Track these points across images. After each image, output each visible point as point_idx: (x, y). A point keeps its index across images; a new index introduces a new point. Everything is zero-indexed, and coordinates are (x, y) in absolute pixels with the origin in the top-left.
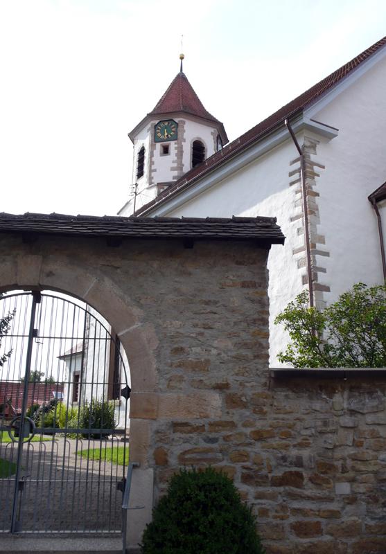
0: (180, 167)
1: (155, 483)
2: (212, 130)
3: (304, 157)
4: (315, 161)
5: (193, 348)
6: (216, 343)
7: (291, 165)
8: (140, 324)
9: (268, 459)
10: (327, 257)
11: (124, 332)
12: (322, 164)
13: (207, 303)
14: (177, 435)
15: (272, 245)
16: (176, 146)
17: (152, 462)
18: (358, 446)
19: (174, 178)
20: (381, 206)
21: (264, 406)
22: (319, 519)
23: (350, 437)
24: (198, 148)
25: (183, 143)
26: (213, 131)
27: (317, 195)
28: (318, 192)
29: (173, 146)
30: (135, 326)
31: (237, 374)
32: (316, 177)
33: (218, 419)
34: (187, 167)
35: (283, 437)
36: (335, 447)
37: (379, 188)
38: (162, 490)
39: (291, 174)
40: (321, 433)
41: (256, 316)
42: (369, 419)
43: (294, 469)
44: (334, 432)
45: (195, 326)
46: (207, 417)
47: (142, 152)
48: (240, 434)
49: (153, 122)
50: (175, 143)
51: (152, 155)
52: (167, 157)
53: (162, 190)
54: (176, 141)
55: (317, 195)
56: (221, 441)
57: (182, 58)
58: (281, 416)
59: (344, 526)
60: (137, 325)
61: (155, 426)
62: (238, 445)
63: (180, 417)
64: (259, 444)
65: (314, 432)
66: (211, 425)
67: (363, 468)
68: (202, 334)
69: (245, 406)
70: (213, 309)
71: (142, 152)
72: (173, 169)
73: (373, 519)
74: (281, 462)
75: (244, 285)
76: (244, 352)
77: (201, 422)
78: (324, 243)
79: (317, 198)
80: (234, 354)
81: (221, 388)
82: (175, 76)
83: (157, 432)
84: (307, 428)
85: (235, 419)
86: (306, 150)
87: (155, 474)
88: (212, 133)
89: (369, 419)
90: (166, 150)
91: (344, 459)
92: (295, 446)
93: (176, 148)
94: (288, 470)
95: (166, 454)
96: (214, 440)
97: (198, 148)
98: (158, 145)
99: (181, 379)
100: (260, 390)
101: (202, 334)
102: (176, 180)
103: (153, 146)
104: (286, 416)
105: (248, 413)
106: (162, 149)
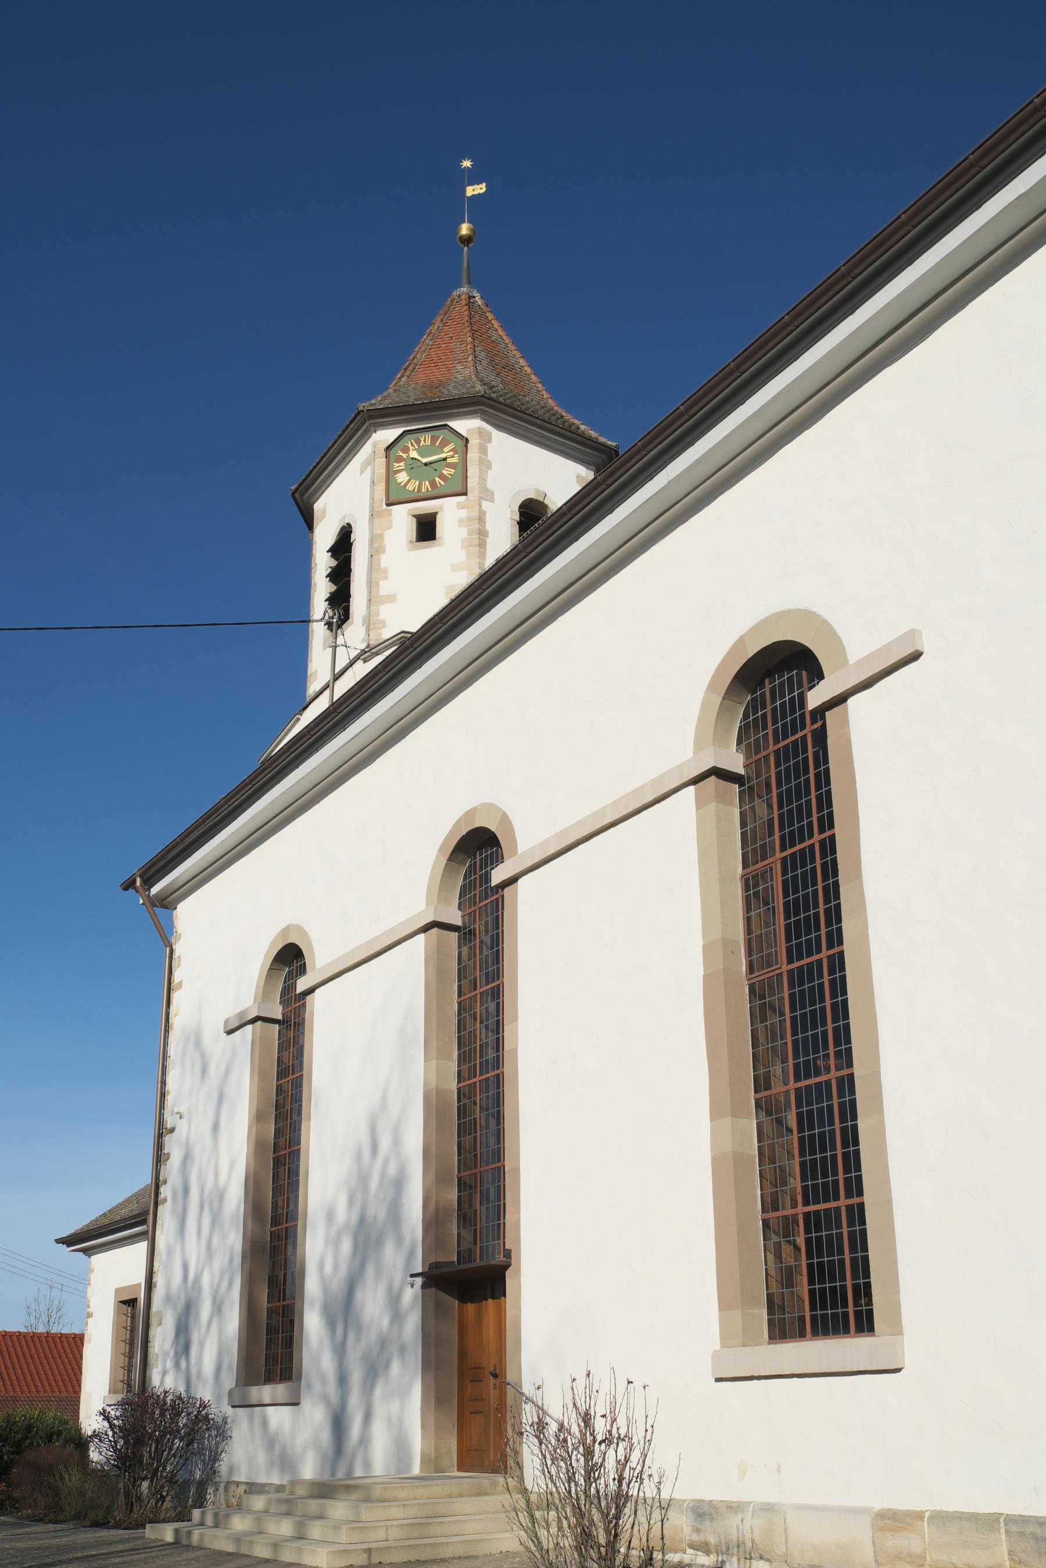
16: (464, 513)
50: (460, 506)
52: (428, 551)
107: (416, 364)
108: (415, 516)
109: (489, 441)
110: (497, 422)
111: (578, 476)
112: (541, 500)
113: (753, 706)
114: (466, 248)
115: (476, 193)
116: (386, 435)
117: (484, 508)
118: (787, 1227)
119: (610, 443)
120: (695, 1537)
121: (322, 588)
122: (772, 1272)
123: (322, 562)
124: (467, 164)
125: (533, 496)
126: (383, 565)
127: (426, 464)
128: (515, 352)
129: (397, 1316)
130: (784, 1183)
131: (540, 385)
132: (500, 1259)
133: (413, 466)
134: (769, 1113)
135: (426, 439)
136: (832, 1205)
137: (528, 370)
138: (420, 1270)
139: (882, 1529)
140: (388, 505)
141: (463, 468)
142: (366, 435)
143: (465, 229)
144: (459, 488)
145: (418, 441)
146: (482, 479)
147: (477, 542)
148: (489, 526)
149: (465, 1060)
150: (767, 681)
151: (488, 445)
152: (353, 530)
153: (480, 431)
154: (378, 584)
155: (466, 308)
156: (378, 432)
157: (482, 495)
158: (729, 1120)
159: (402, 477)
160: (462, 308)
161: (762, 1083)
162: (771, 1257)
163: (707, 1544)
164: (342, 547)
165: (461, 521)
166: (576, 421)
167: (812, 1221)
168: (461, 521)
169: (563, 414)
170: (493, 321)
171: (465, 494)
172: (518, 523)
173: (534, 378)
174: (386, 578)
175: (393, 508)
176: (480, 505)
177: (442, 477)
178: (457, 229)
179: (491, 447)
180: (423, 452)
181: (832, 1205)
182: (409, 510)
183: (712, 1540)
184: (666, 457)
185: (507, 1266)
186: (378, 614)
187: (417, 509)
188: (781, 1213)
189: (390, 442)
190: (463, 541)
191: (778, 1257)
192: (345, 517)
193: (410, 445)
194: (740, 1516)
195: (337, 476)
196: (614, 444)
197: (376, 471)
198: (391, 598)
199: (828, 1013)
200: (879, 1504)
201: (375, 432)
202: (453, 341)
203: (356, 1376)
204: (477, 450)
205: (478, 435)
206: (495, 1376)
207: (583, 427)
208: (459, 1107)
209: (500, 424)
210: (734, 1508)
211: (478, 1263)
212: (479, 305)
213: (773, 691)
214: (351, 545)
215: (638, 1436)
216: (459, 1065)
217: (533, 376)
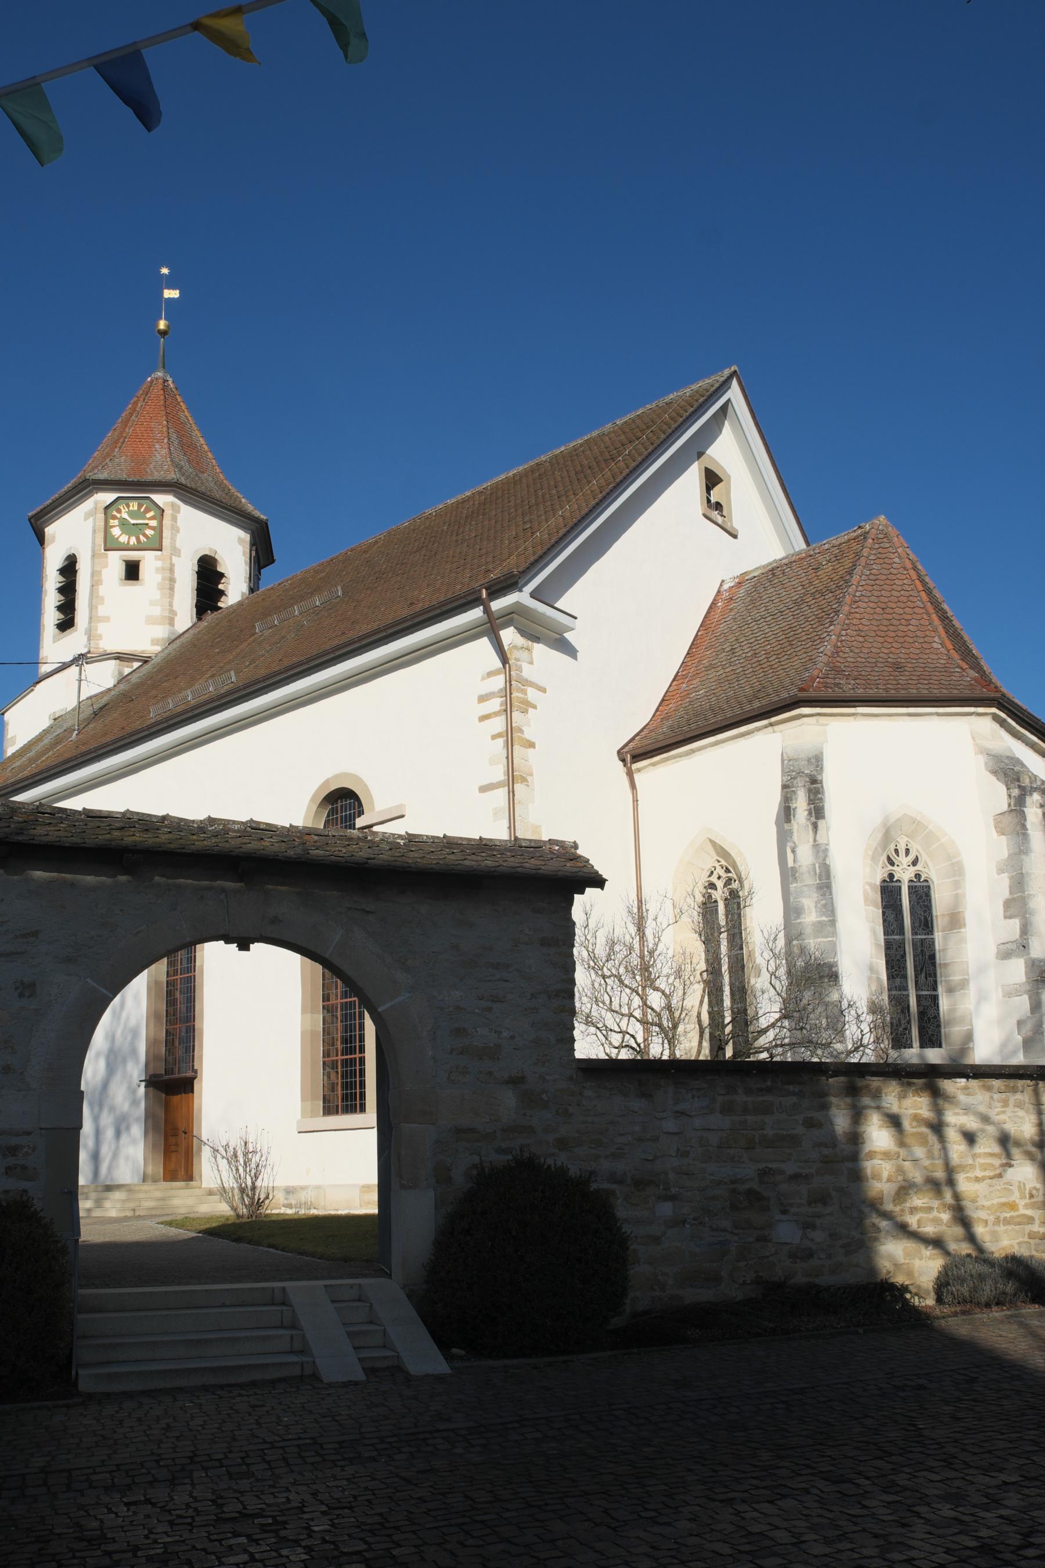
4: (529, 679)
5: (477, 1029)
7: (483, 679)
11: (388, 1005)
12: (542, 684)
15: (587, 889)
16: (159, 564)
19: (154, 642)
21: (570, 1105)
27: (531, 745)
28: (533, 740)
29: (149, 561)
30: (401, 998)
32: (530, 710)
35: (593, 1146)
37: (637, 735)
39: (482, 699)
45: (481, 998)
50: (157, 558)
51: (95, 575)
52: (132, 588)
53: (127, 671)
55: (531, 745)
65: (630, 1139)
68: (490, 1009)
72: (150, 620)
79: (531, 750)
81: (515, 1081)
84: (622, 1135)
87: (435, 1195)
89: (697, 1122)
90: (132, 571)
101: (490, 1009)
107: (125, 437)
108: (124, 561)
109: (179, 512)
110: (184, 498)
111: (239, 538)
112: (213, 556)
113: (332, 812)
114: (162, 339)
115: (171, 296)
116: (107, 497)
117: (173, 561)
118: (334, 1065)
119: (262, 517)
120: (286, 1202)
121: (51, 599)
122: (326, 1085)
123: (52, 580)
124: (165, 271)
125: (207, 553)
126: (101, 594)
127: (134, 524)
128: (197, 432)
129: (135, 1103)
130: (333, 1045)
131: (214, 461)
132: (190, 1074)
133: (123, 524)
134: (328, 1011)
135: (134, 506)
136: (353, 1056)
137: (206, 448)
138: (144, 1079)
139: (364, 1192)
140: (105, 550)
141: (159, 530)
142: (89, 494)
143: (162, 325)
144: (157, 546)
145: (128, 506)
146: (173, 540)
147: (168, 586)
148: (177, 575)
149: (171, 965)
150: (339, 801)
151: (178, 515)
152: (78, 560)
153: (173, 505)
154: (97, 608)
155: (162, 392)
156: (99, 494)
157: (172, 552)
158: (310, 1015)
159: (116, 532)
160: (157, 391)
161: (326, 998)
162: (326, 1078)
163: (291, 1204)
164: (69, 569)
165: (157, 569)
166: (239, 495)
167: (345, 1063)
168: (157, 569)
169: (230, 487)
170: (181, 403)
171: (161, 550)
172: (197, 573)
173: (210, 455)
174: (102, 604)
175: (109, 552)
176: (171, 560)
177: (145, 535)
178: (157, 325)
179: (180, 517)
180: (132, 514)
181: (353, 1056)
182: (121, 556)
183: (293, 1202)
184: (295, 678)
185: (195, 1078)
186: (96, 629)
187: (125, 556)
188: (331, 1059)
189: (108, 503)
190: (159, 584)
191: (329, 1077)
192: (71, 548)
193: (122, 508)
194: (306, 1192)
195: (65, 514)
196: (265, 518)
197: (97, 523)
198: (107, 619)
199: (164, 1290)
200: (363, 1183)
201: (97, 493)
202: (152, 420)
203: (109, 1133)
204: (170, 518)
205: (171, 508)
206: (185, 1133)
207: (243, 500)
208: (167, 991)
209: (186, 500)
210: (303, 1188)
211: (176, 1076)
212: (171, 389)
213: (342, 806)
214: (76, 571)
215: (264, 1152)
216: (168, 968)
217: (209, 453)
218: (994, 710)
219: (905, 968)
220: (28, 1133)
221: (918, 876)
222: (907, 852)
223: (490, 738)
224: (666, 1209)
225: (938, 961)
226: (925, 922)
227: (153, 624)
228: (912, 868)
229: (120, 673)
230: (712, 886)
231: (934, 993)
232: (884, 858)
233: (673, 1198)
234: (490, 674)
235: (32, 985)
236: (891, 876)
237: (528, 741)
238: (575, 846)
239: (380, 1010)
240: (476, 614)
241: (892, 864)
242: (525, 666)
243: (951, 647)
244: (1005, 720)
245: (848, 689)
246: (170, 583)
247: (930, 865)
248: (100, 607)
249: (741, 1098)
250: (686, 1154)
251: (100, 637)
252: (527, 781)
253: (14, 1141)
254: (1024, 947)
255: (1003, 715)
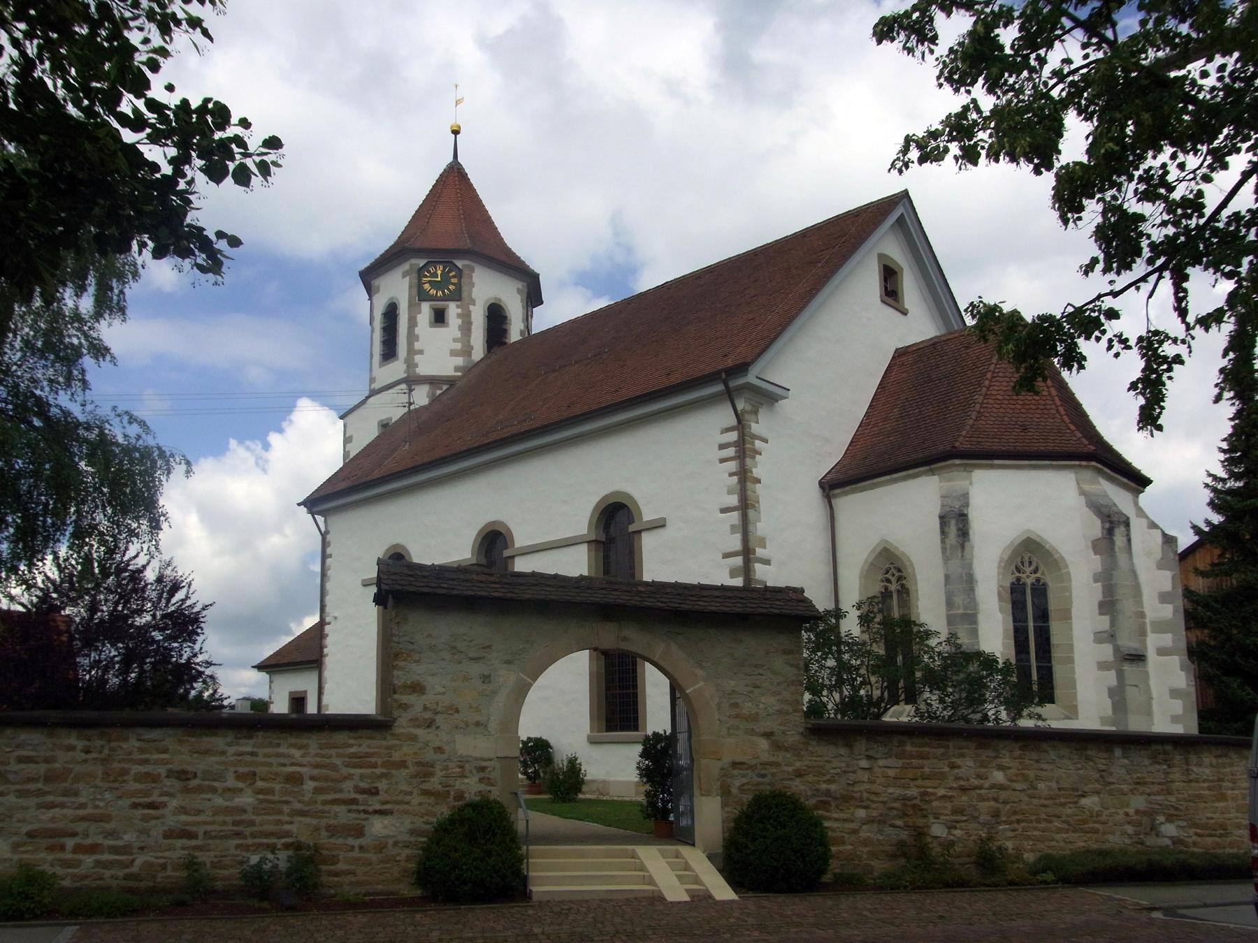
0: (467, 351)
1: (722, 807)
2: (520, 285)
3: (743, 428)
6: (763, 700)
7: (722, 433)
8: (703, 683)
9: (805, 790)
10: (768, 566)
11: (691, 689)
13: (756, 666)
14: (736, 772)
16: (459, 311)
17: (719, 791)
18: (871, 782)
19: (456, 369)
20: (835, 496)
22: (844, 835)
23: (864, 776)
24: (496, 317)
25: (471, 307)
26: (520, 287)
27: (758, 481)
29: (453, 310)
30: (699, 685)
31: (780, 725)
33: (766, 760)
34: (478, 352)
36: (855, 782)
38: (728, 812)
39: (722, 447)
40: (845, 772)
41: (794, 678)
42: (881, 763)
43: (825, 799)
44: (854, 772)
45: (747, 685)
46: (758, 758)
47: (391, 314)
48: (784, 771)
49: (414, 261)
52: (440, 331)
53: (439, 392)
54: (459, 303)
55: (758, 481)
56: (769, 776)
57: (456, 132)
58: (814, 759)
59: (861, 839)
60: (701, 684)
61: (720, 764)
62: (783, 780)
63: (739, 758)
64: (798, 780)
66: (761, 764)
67: (875, 799)
69: (786, 750)
70: (761, 671)
71: (391, 314)
72: (454, 353)
73: (881, 835)
74: (815, 792)
75: (785, 652)
76: (786, 707)
77: (754, 762)
78: (765, 547)
79: (758, 485)
80: (777, 708)
81: (768, 735)
82: (444, 166)
83: (722, 769)
85: (780, 760)
86: (747, 417)
88: (519, 291)
90: (439, 318)
91: (861, 792)
92: (824, 782)
93: (459, 316)
94: (820, 799)
95: (729, 786)
96: (764, 776)
97: (496, 317)
98: (426, 308)
99: (737, 728)
100: (797, 738)
102: (459, 374)
103: (414, 308)
104: (818, 759)
105: (789, 756)
106: (433, 313)
159: (427, 286)
174: (418, 341)
177: (448, 289)
190: (460, 326)
198: (421, 352)
218: (1093, 463)
219: (1028, 646)
220: (491, 760)
221: (1038, 580)
222: (1030, 563)
223: (717, 447)
224: (861, 813)
225: (1052, 643)
226: (1043, 615)
227: (456, 356)
228: (1034, 576)
229: (434, 394)
230: (888, 581)
231: (1049, 665)
232: (1013, 567)
233: (866, 807)
234: (727, 430)
235: (489, 676)
236: (1018, 579)
237: (756, 478)
238: (802, 590)
239: (688, 691)
240: (720, 387)
241: (1019, 572)
242: (753, 425)
243: (1063, 412)
244: (1102, 469)
245: (987, 445)
246: (466, 327)
247: (1046, 574)
248: (416, 343)
249: (909, 748)
250: (874, 782)
251: (416, 365)
252: (755, 507)
253: (484, 764)
254: (1112, 636)
255: (1099, 466)
